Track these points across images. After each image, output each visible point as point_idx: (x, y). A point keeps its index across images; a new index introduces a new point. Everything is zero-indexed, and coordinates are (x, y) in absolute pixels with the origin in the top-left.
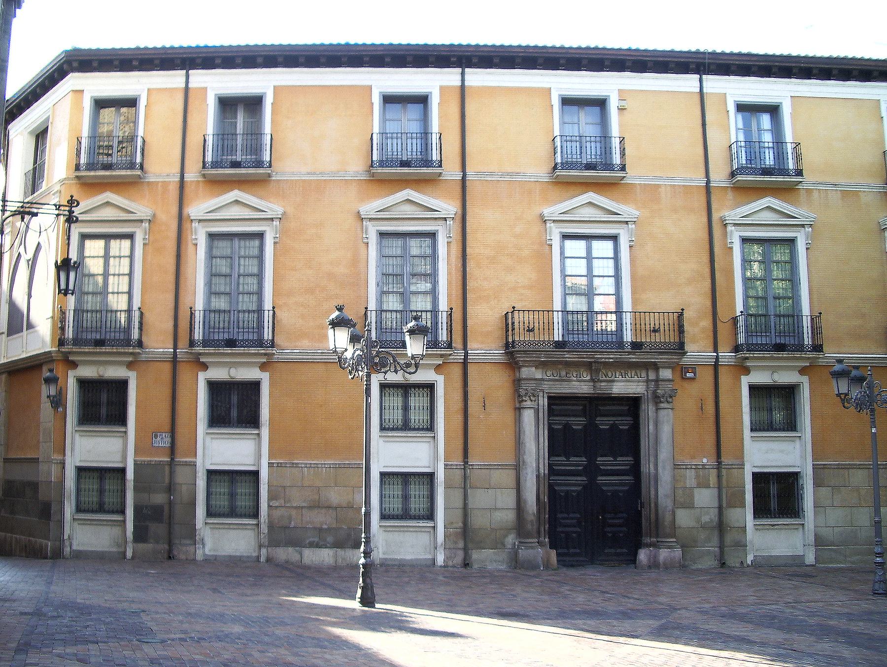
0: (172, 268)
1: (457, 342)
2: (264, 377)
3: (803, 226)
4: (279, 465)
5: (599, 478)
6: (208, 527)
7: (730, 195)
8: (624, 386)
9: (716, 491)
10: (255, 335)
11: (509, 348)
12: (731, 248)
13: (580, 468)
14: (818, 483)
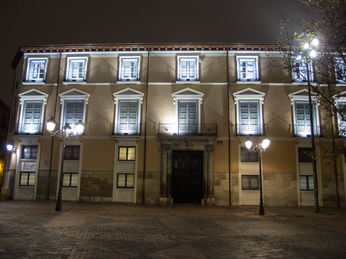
1: (64, 251)
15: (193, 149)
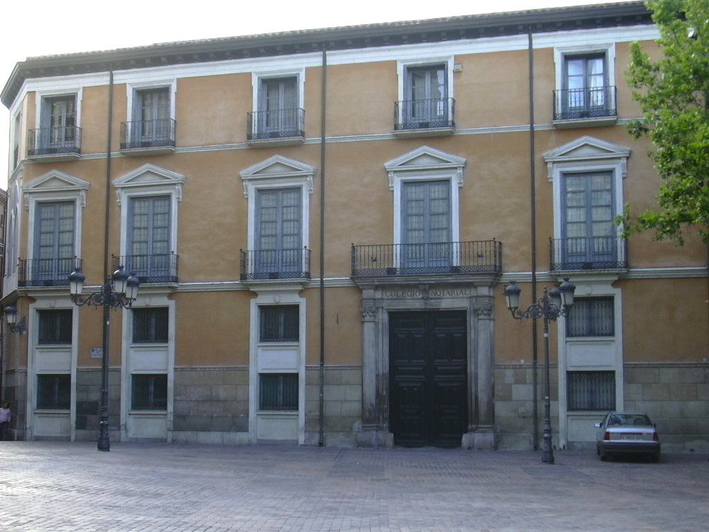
0: (103, 225)
2: (171, 304)
3: (619, 158)
4: (182, 369)
5: (437, 377)
6: (131, 416)
7: (553, 137)
8: (450, 301)
9: (531, 387)
10: (296, 267)
11: (354, 275)
12: (551, 183)
13: (421, 368)
14: (628, 380)
15: (439, 309)
